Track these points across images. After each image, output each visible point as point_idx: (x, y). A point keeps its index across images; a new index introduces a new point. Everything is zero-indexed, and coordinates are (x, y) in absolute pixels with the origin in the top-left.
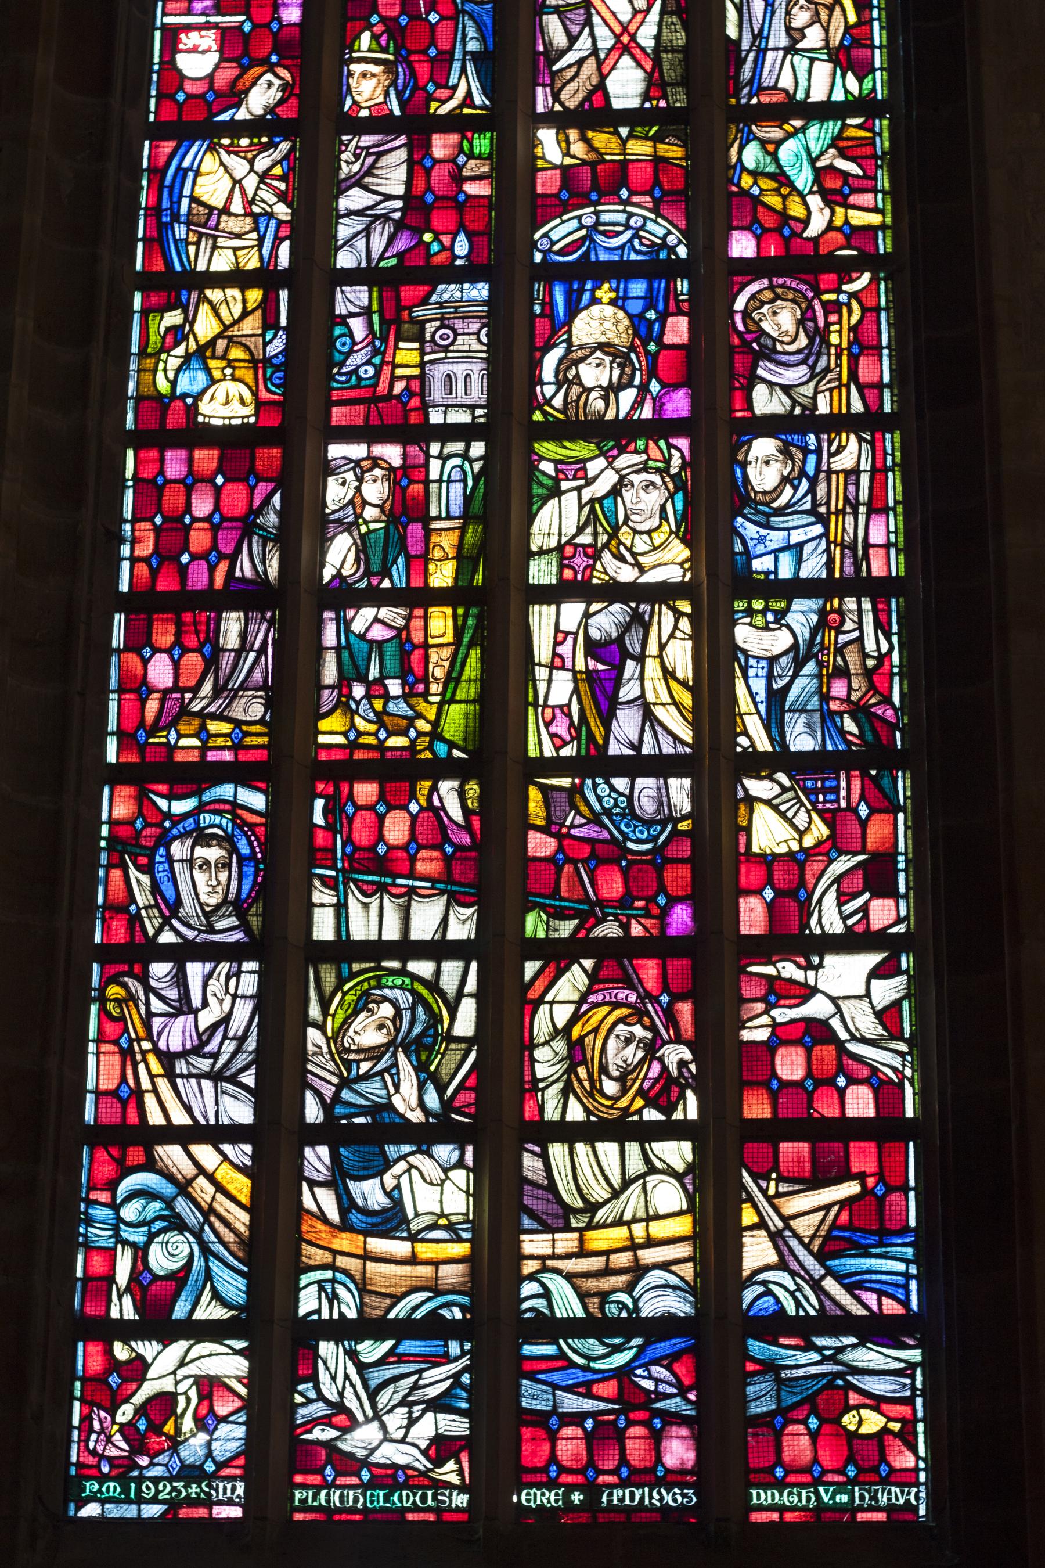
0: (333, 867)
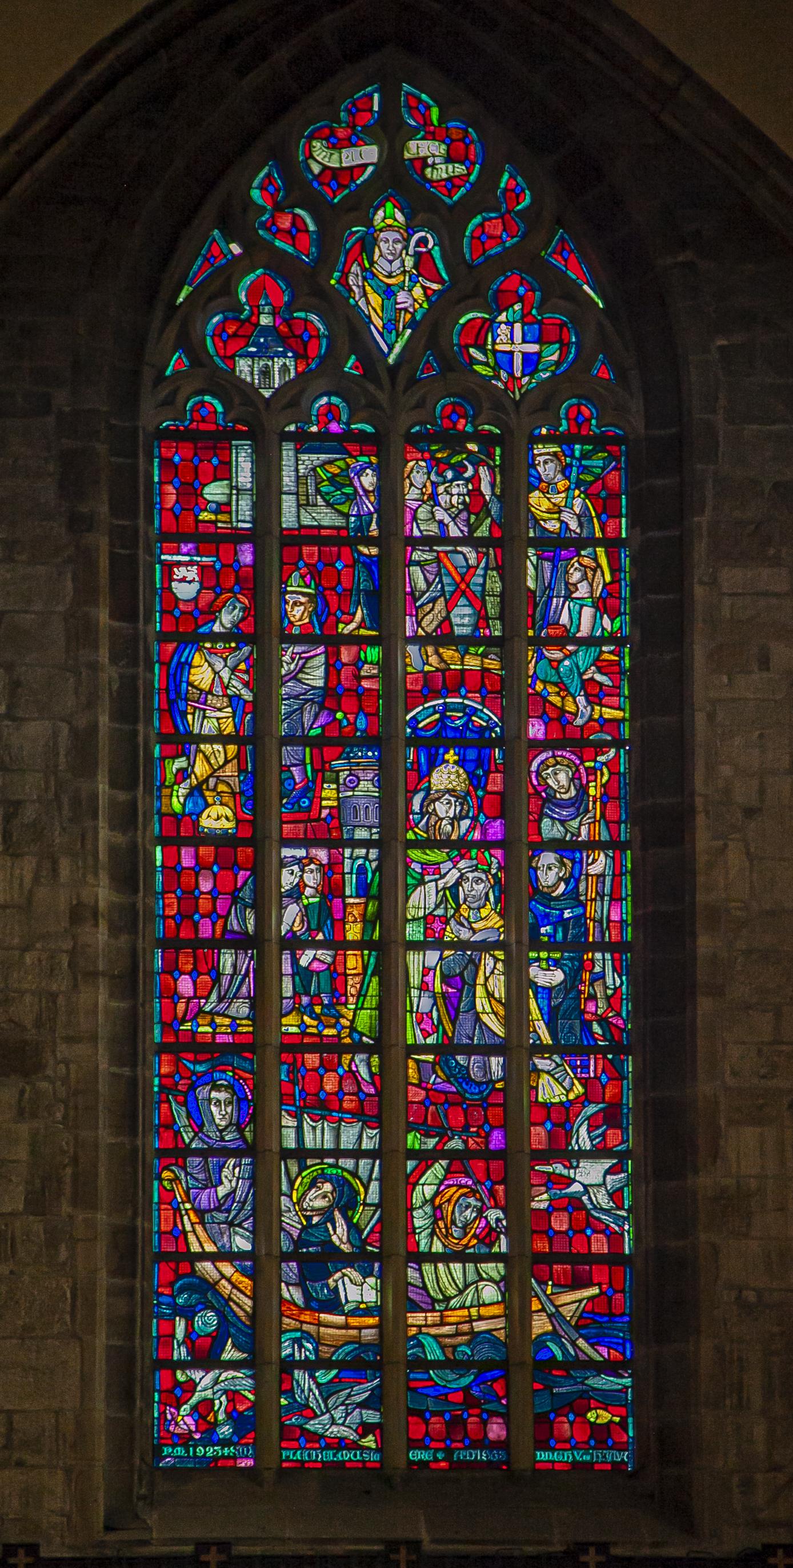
0: (294, 1105)
